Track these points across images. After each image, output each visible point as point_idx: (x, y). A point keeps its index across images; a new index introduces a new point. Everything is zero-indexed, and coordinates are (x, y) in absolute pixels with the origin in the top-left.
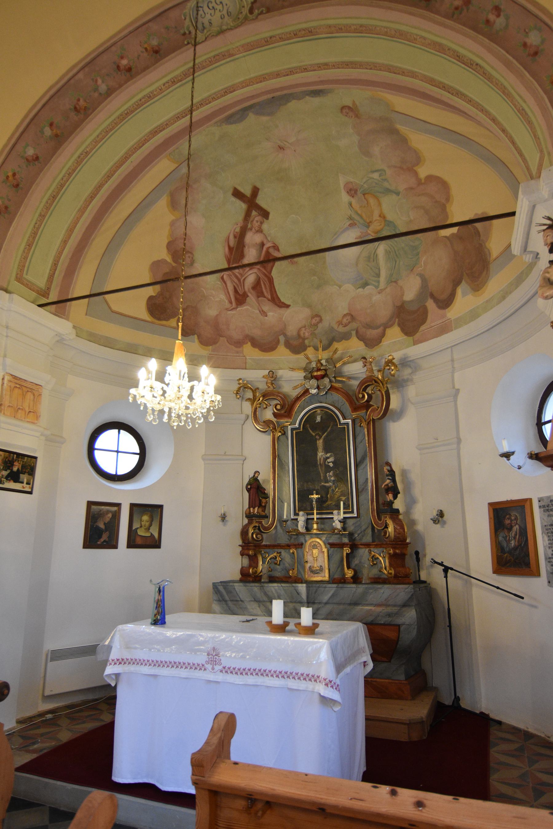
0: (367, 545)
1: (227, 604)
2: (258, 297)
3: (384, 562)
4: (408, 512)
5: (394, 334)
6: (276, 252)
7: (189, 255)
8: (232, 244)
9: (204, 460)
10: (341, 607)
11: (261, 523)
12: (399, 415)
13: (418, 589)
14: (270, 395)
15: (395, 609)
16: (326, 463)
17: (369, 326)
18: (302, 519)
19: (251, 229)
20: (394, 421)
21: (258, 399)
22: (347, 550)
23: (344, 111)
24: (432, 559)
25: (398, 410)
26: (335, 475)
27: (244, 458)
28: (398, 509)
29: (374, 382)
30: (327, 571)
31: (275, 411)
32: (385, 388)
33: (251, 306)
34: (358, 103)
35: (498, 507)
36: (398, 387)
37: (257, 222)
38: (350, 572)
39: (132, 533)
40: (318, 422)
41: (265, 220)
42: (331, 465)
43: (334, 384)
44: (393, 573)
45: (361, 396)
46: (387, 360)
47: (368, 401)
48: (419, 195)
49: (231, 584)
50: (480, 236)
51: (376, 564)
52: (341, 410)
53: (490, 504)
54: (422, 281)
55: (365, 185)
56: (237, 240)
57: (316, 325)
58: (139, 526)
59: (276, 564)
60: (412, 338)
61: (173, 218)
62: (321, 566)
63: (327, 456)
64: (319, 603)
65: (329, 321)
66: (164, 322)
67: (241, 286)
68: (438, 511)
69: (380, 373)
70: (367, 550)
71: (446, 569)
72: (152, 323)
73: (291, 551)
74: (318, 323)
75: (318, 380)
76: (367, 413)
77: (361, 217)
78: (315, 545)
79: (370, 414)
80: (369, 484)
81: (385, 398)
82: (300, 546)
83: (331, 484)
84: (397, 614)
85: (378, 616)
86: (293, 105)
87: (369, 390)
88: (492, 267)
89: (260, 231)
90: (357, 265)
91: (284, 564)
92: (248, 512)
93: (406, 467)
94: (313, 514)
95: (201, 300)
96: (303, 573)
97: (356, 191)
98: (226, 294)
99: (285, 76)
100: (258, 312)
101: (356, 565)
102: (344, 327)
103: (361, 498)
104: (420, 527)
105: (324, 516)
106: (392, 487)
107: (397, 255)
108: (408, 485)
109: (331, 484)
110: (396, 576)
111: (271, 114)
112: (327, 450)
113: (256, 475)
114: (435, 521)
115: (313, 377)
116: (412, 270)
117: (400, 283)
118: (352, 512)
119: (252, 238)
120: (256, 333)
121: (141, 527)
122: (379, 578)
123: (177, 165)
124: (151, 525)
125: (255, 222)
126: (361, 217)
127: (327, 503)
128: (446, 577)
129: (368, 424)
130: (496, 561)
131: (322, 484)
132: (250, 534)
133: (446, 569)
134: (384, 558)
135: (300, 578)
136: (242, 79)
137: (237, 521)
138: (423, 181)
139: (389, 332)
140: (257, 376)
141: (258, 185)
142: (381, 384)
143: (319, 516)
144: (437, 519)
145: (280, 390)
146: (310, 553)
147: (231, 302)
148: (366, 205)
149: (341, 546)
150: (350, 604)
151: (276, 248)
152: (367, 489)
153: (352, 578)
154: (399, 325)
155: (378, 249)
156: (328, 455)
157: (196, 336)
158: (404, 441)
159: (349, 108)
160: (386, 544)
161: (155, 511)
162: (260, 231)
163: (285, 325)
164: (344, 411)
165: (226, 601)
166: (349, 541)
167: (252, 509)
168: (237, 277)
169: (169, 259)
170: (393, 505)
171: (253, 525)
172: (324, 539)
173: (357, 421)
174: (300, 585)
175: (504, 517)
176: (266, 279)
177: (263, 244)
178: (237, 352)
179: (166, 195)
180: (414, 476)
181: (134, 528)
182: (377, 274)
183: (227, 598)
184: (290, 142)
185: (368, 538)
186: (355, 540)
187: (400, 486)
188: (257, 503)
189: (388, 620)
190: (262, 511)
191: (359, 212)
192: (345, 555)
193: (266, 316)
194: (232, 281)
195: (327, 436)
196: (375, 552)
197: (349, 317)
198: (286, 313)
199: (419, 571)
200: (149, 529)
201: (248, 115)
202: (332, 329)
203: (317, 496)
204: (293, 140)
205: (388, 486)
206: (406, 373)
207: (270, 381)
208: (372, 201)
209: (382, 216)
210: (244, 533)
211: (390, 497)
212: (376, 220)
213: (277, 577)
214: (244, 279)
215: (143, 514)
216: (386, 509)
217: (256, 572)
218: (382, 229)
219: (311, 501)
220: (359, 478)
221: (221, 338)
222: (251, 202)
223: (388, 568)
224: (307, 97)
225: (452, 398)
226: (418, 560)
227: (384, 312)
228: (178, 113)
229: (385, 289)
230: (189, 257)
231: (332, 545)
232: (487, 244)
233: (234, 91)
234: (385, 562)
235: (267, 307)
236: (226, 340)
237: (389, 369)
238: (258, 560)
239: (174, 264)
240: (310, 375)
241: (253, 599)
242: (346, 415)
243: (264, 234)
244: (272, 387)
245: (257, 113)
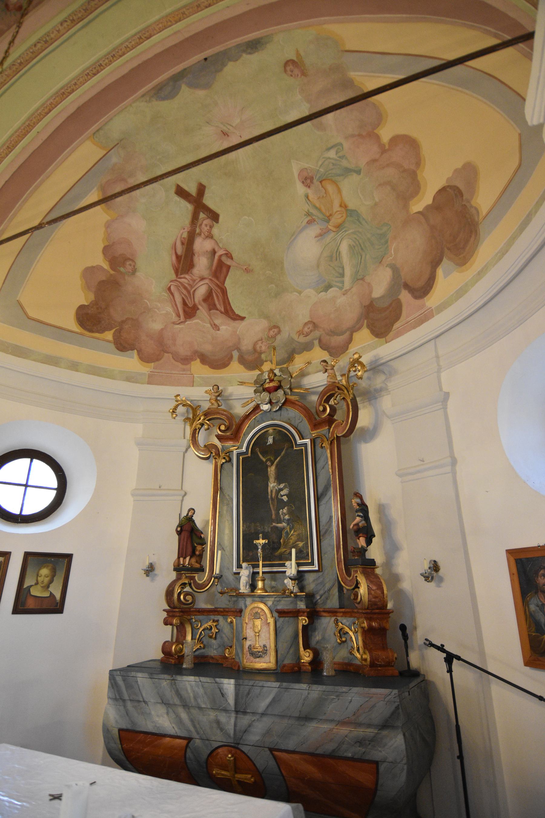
0: (332, 612)
1: (125, 707)
2: (210, 310)
3: (356, 639)
4: (389, 564)
5: (364, 336)
6: (229, 259)
7: (130, 262)
8: (179, 252)
9: (133, 495)
10: (286, 721)
11: (193, 578)
12: (369, 434)
13: (407, 694)
14: (214, 414)
15: (370, 732)
16: (279, 497)
17: (333, 333)
18: (245, 573)
19: (200, 234)
20: (366, 442)
21: (198, 418)
22: (303, 620)
23: (288, 68)
24: (426, 640)
25: (371, 428)
26: (290, 513)
27: (183, 493)
28: (373, 560)
29: (337, 390)
30: (273, 653)
31: (219, 433)
32: (352, 396)
33: (203, 318)
34: (302, 54)
35: (522, 556)
36: (370, 400)
37: (206, 225)
38: (307, 654)
39: (22, 592)
40: (270, 444)
41: (214, 223)
42: (285, 498)
43: (288, 397)
44: (369, 659)
45: (321, 408)
46: (351, 360)
47: (331, 415)
48: (384, 168)
49: (133, 674)
50: (462, 196)
51: (346, 641)
52: (299, 428)
53: (510, 552)
54: (393, 272)
55: (322, 170)
56: (185, 247)
57: (274, 337)
58: (33, 584)
59: (211, 637)
60: (384, 339)
61: (109, 218)
62: (265, 646)
63: (279, 487)
64: (253, 713)
65: (288, 331)
66: (97, 335)
67: (191, 298)
68: (430, 562)
69: (344, 378)
70: (333, 619)
71: (450, 658)
72: (81, 334)
73: (229, 620)
74: (276, 335)
75: (270, 393)
76: (329, 429)
77: (319, 210)
78: (257, 613)
79: (333, 432)
80: (334, 524)
81: (351, 409)
82: (239, 613)
83: (284, 524)
84: (373, 741)
85: (343, 743)
86: (231, 68)
87: (332, 402)
88: (482, 228)
89: (210, 236)
90: (318, 266)
91: (222, 637)
92: (176, 564)
93: (384, 501)
94: (258, 566)
95: (145, 312)
96: (240, 655)
97: (312, 179)
98: (172, 306)
99: (206, 7)
100: (209, 325)
101: (318, 642)
102: (306, 336)
103: (324, 543)
104: (406, 585)
105: (275, 569)
106: (364, 527)
107: (362, 249)
108: (388, 526)
109: (284, 524)
110: (373, 665)
111: (207, 86)
112: (279, 479)
113: (190, 514)
114: (428, 578)
115: (265, 390)
116: (380, 262)
117: (368, 279)
118: (312, 564)
119: (201, 245)
120: (207, 348)
121: (37, 584)
122: (349, 664)
123: (105, 152)
124: (51, 581)
125: (203, 226)
126: (319, 210)
127: (279, 551)
128: (450, 671)
129: (332, 443)
130: (528, 646)
131: (274, 524)
132: (176, 595)
133: (450, 658)
134: (355, 632)
135: (237, 663)
136: (157, 17)
137: (167, 576)
138: (387, 147)
139: (356, 336)
140: (199, 395)
141: (204, 182)
142: (346, 391)
143: (266, 569)
144: (430, 573)
145: (231, 411)
146: (250, 625)
147: (179, 316)
148: (325, 195)
149: (296, 614)
150: (299, 718)
151: (229, 255)
152: (331, 531)
153: (311, 663)
154: (368, 327)
155: (341, 246)
156: (282, 486)
157: (135, 351)
158: (380, 467)
159: (292, 62)
160: (358, 612)
161: (61, 562)
162: (210, 236)
163: (239, 339)
164: (301, 428)
165: (124, 701)
166: (307, 607)
167: (181, 559)
168: (185, 288)
169: (106, 266)
170: (367, 553)
171: (181, 582)
172: (270, 603)
173: (318, 441)
174: (225, 681)
175: (537, 573)
176: (219, 291)
177: (214, 252)
178: (184, 370)
179: (95, 189)
180: (395, 513)
181: (25, 586)
182: (340, 274)
183: (126, 697)
184: (234, 125)
185: (334, 602)
186: (316, 604)
187: (376, 527)
188: (190, 550)
189: (358, 751)
190: (197, 562)
191: (317, 205)
192: (300, 627)
193: (219, 330)
194: (181, 293)
195: (279, 461)
196: (345, 622)
197: (310, 326)
198: (241, 326)
199: (407, 655)
200: (48, 587)
201: (180, 87)
202: (292, 340)
203: (264, 541)
204: (236, 121)
205: (360, 527)
206: (379, 381)
207: (214, 397)
208: (330, 188)
209: (343, 205)
210: (169, 593)
211: (362, 542)
212: (336, 212)
213: (212, 658)
214: (195, 291)
215: (41, 566)
216: (357, 560)
217: (181, 650)
218: (344, 222)
219: (256, 547)
220: (321, 515)
221: (166, 354)
222: (197, 200)
223: (361, 650)
224: (244, 55)
225: (440, 404)
226: (405, 637)
227: (351, 315)
228: (88, 68)
229: (350, 289)
230: (130, 265)
231: (282, 613)
232: (473, 203)
233: (151, 36)
234: (357, 639)
235: (220, 320)
236: (171, 356)
237: (355, 371)
238: (185, 631)
239: (112, 272)
240: (261, 388)
241: (160, 701)
242: (304, 435)
243: (214, 240)
244: (216, 405)
245: (192, 86)
